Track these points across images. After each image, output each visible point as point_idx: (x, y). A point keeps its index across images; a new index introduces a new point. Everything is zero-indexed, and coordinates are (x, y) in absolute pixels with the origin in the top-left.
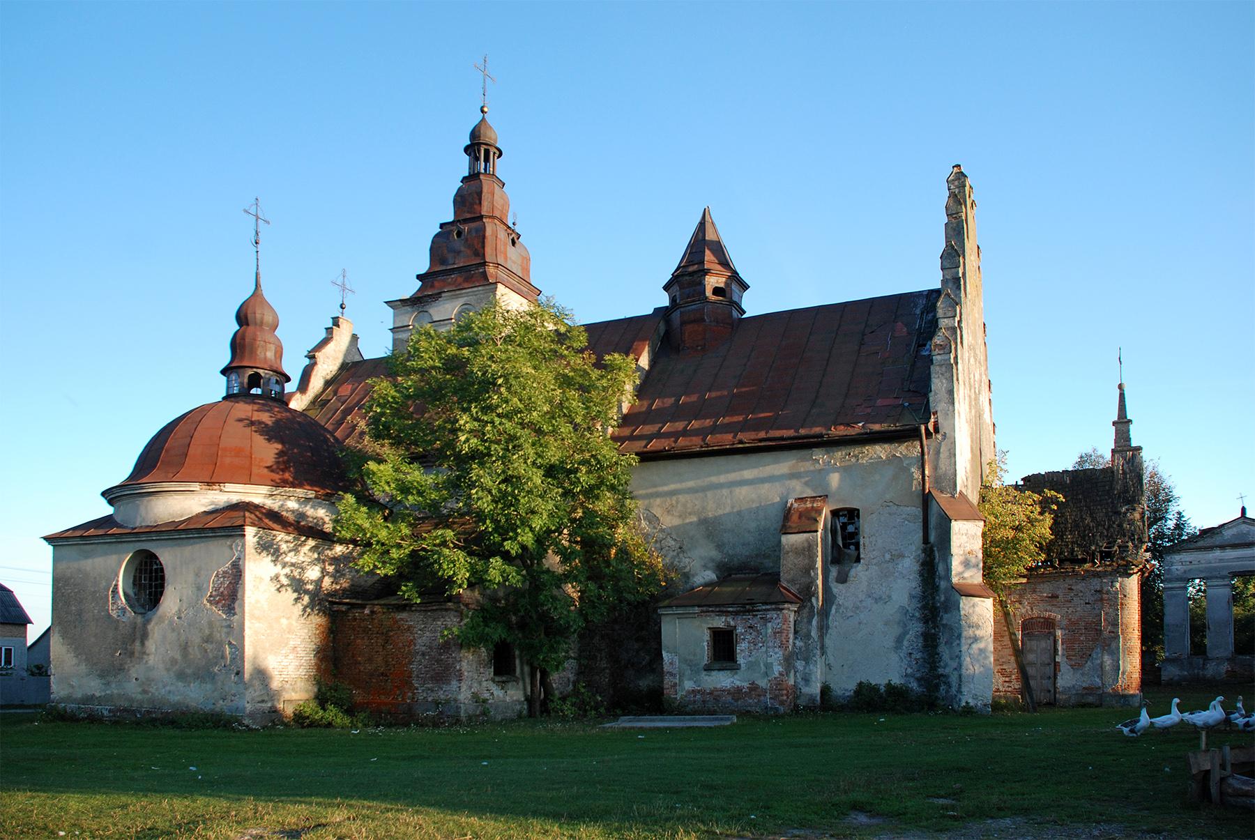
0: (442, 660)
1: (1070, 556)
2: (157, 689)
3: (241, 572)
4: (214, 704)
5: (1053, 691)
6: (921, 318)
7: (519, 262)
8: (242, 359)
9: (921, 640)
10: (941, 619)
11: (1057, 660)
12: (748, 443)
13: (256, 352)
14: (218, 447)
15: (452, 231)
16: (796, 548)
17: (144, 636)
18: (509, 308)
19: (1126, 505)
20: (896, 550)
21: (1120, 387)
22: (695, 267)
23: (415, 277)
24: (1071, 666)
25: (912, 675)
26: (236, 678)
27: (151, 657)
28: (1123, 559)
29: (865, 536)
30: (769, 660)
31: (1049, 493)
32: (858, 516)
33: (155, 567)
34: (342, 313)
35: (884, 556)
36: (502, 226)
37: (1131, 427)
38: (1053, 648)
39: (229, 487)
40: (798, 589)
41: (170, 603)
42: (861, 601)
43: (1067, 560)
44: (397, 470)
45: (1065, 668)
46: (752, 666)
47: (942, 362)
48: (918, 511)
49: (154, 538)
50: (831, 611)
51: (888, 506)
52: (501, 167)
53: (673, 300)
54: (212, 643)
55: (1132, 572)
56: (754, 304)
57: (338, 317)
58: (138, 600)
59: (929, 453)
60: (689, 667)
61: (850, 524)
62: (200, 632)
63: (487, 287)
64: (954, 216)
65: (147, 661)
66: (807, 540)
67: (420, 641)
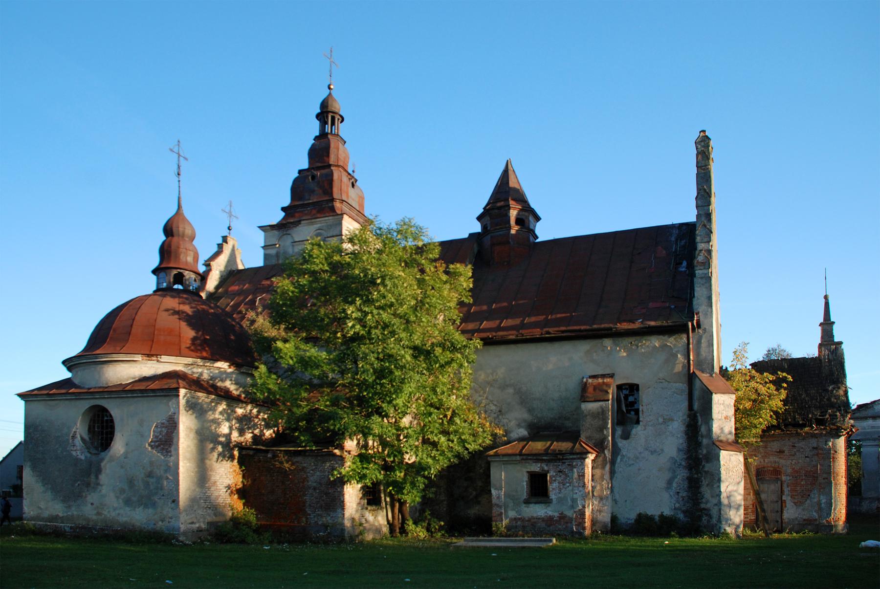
0: (330, 493)
1: (793, 422)
2: (109, 512)
3: (176, 423)
4: (155, 524)
5: (780, 521)
6: (676, 244)
7: (357, 200)
8: (169, 261)
9: (686, 483)
10: (704, 467)
11: (783, 499)
12: (554, 334)
13: (179, 257)
14: (155, 328)
15: (308, 176)
16: (593, 413)
17: (99, 471)
18: (381, 226)
19: (832, 385)
20: (667, 415)
21: (826, 297)
22: (502, 203)
23: (280, 208)
24: (794, 503)
25: (679, 509)
26: (173, 505)
27: (104, 487)
28: (834, 424)
29: (644, 404)
30: (575, 496)
31: (782, 374)
32: (638, 389)
33: (106, 418)
34: (229, 233)
35: (658, 420)
36: (345, 173)
37: (834, 327)
38: (780, 489)
39: (164, 358)
40: (594, 444)
41: (118, 446)
42: (640, 453)
43: (790, 424)
44: (297, 348)
45: (789, 503)
46: (561, 501)
47: (703, 276)
48: (684, 387)
49: (106, 396)
50: (617, 460)
51: (661, 382)
52: (343, 129)
53: (484, 227)
54: (153, 477)
55: (842, 434)
56: (544, 232)
57: (227, 236)
58: (92, 443)
59: (693, 343)
60: (512, 501)
61: (630, 395)
62: (143, 469)
63: (336, 217)
64: (703, 168)
65: (100, 491)
66: (601, 407)
67: (311, 478)
